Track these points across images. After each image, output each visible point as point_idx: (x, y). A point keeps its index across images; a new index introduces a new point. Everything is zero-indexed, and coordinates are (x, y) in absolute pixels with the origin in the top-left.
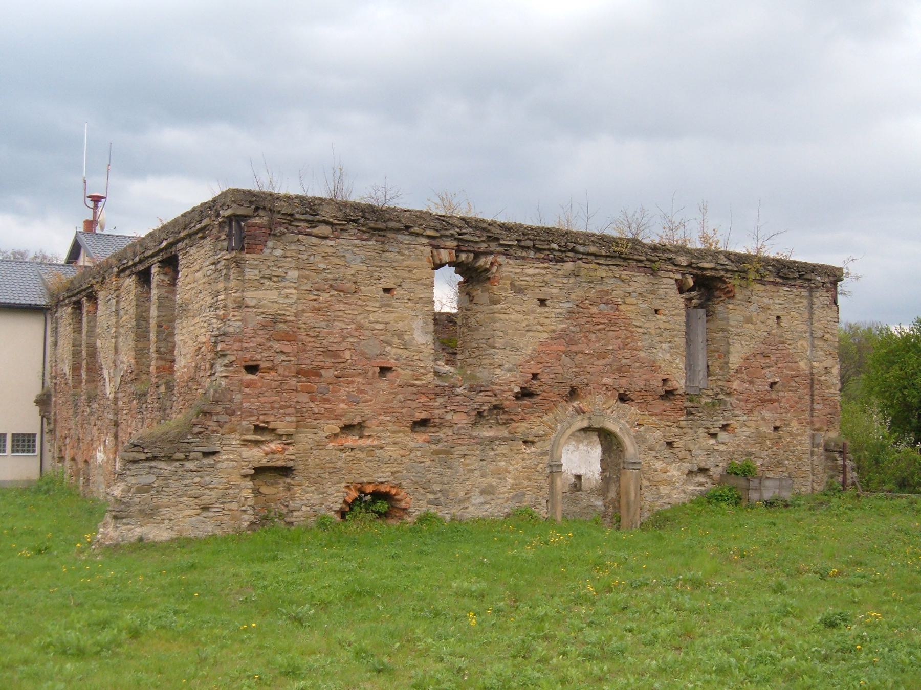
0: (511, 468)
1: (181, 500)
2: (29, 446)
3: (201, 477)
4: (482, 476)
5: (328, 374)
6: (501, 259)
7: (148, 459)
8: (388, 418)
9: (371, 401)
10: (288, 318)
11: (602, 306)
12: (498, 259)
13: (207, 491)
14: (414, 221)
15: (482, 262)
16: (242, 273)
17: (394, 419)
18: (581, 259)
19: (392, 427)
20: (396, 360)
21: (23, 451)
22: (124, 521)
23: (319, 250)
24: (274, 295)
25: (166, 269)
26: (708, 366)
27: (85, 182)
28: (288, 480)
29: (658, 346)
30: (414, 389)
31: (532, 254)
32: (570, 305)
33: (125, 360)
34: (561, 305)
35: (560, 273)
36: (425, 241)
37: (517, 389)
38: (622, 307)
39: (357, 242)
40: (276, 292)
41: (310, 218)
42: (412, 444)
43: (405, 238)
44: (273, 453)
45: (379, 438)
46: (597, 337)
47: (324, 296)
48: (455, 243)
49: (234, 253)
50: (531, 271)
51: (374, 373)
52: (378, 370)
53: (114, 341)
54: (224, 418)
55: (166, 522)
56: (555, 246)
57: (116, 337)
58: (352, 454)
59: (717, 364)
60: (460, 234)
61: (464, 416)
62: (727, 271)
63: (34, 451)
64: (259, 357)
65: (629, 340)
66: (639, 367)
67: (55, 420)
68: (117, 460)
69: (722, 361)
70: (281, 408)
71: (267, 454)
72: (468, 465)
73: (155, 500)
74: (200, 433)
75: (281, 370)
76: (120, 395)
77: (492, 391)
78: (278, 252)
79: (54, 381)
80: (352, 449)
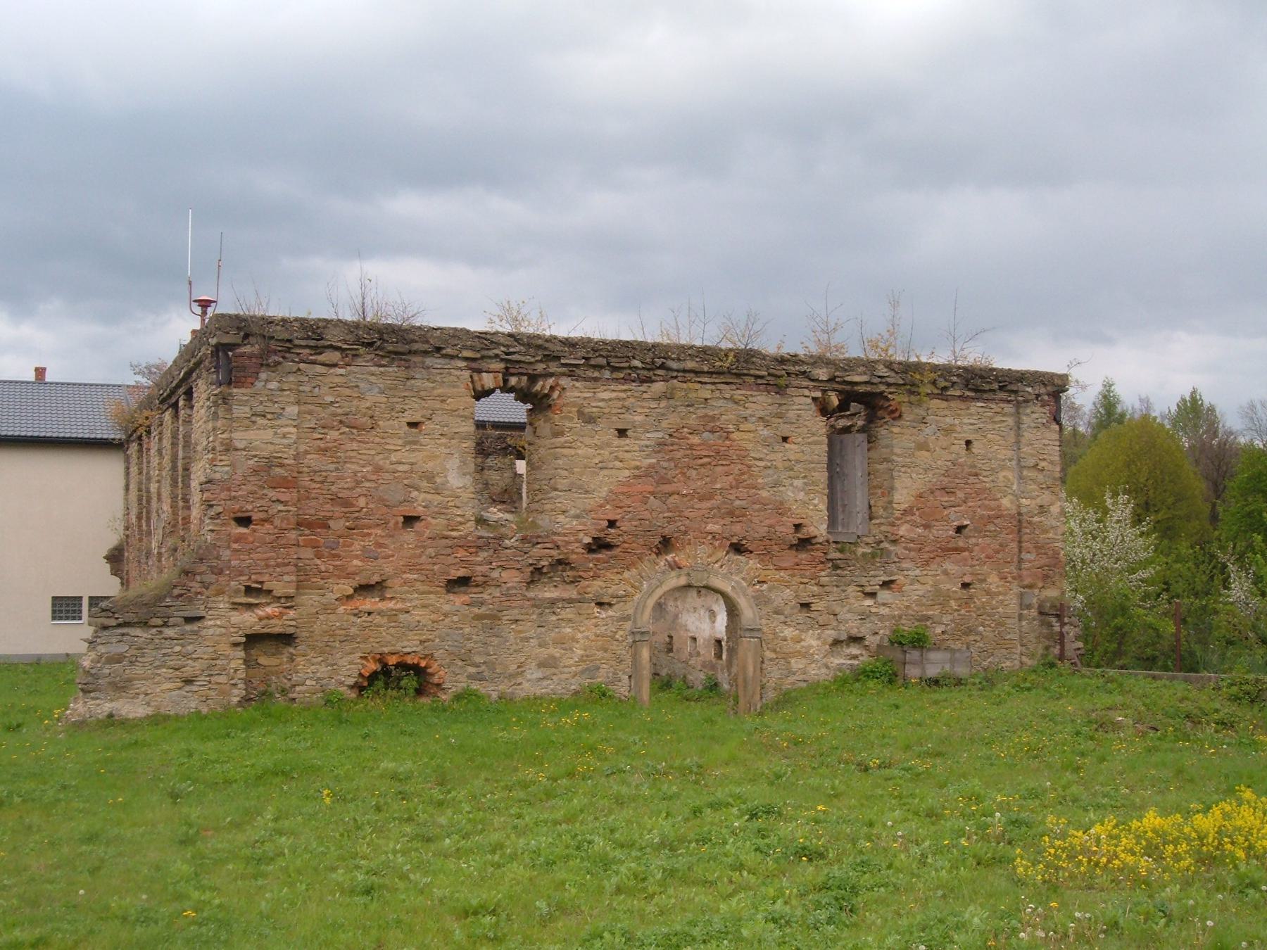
11: (706, 435)
13: (190, 662)
23: (327, 380)
24: (268, 435)
36: (462, 364)
40: (270, 431)
41: (312, 343)
45: (403, 600)
48: (502, 365)
51: (397, 523)
52: (401, 519)
54: (210, 578)
55: (142, 696)
64: (249, 507)
69: (886, 499)
70: (278, 565)
77: (553, 542)
78: (273, 385)
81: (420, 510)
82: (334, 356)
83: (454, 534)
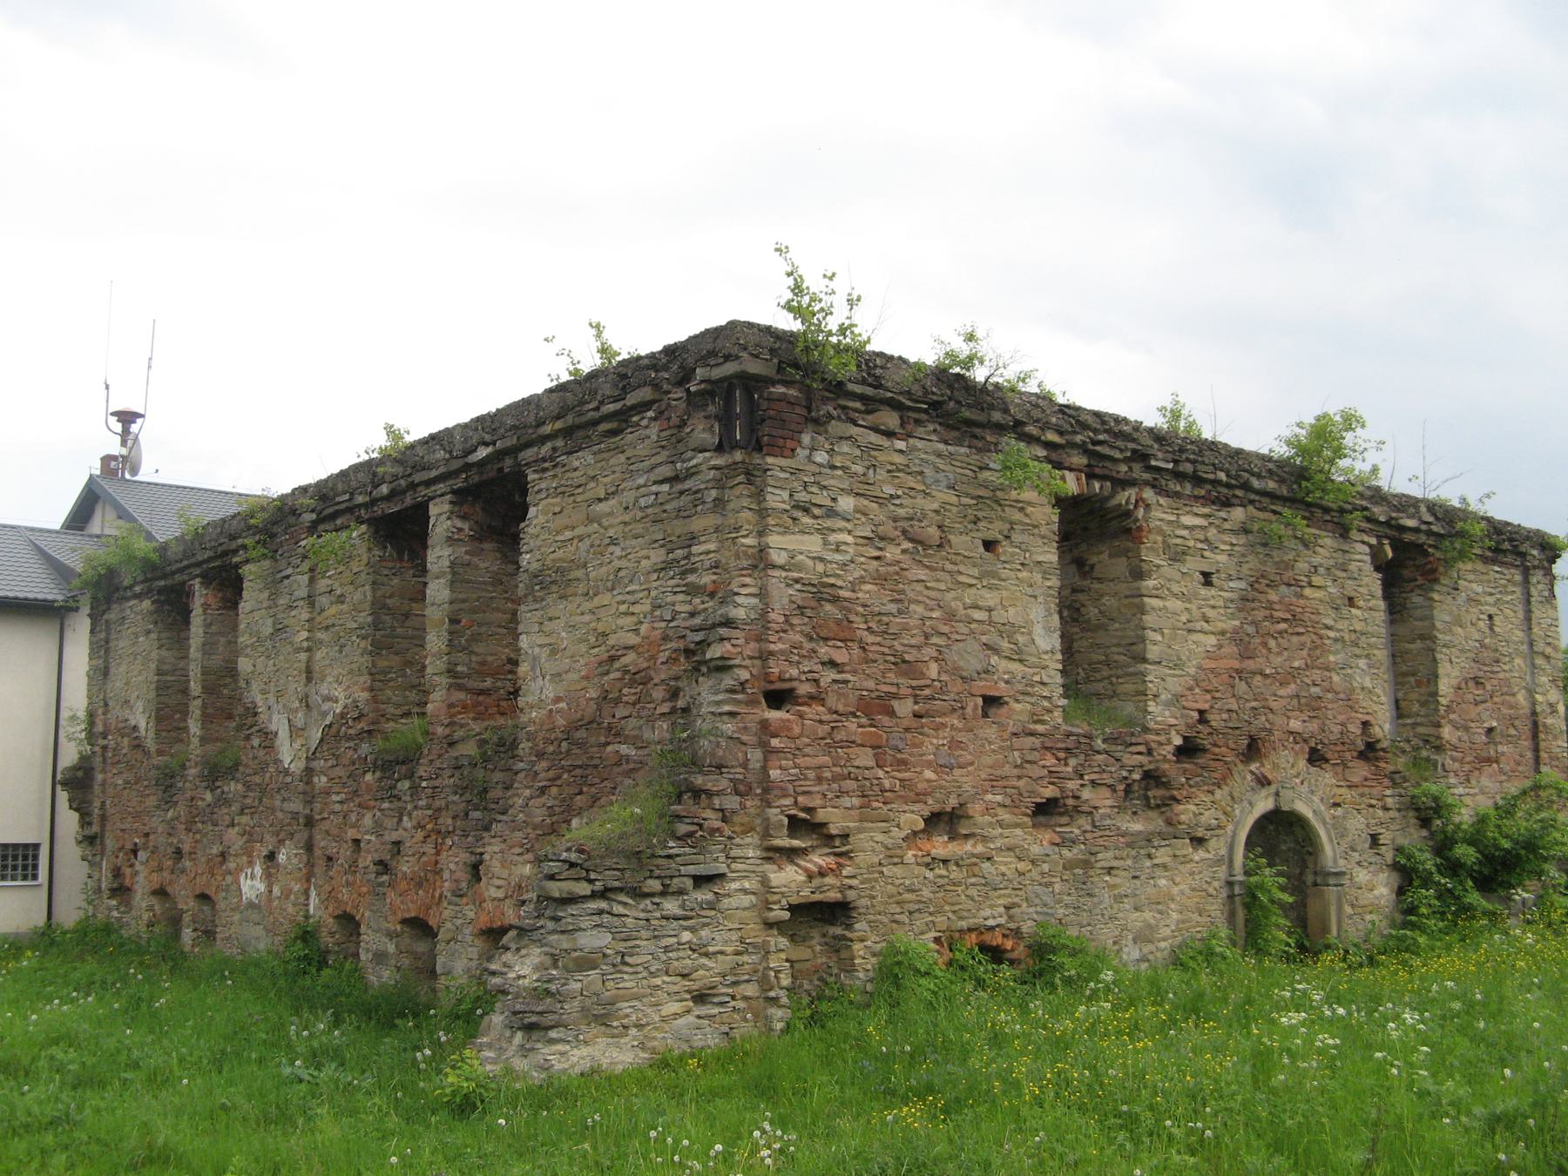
0: (1175, 890)
1: (658, 981)
2: (25, 868)
3: (692, 930)
4: (1136, 909)
5: (904, 708)
6: (1148, 494)
7: (594, 895)
8: (999, 798)
9: (972, 764)
10: (842, 593)
11: (1283, 588)
12: (1145, 495)
13: (704, 961)
14: (1028, 413)
15: (1126, 496)
16: (759, 495)
17: (1008, 801)
18: (1252, 502)
19: (1005, 816)
20: (1007, 682)
21: (14, 878)
22: (553, 1034)
23: (882, 457)
24: (813, 544)
25: (465, 508)
26: (1397, 701)
27: (107, 387)
28: (838, 931)
29: (1353, 661)
30: (1037, 742)
31: (1188, 489)
32: (1242, 585)
33: (339, 693)
34: (1232, 584)
35: (1227, 526)
36: (1042, 452)
37: (1178, 741)
38: (1308, 592)
39: (941, 446)
40: (817, 538)
41: (869, 391)
42: (1036, 849)
43: (1010, 442)
44: (822, 874)
45: (985, 839)
46: (1278, 645)
47: (892, 553)
48: (1085, 461)
49: (738, 456)
50: (1187, 520)
52: (980, 701)
53: (303, 656)
54: (731, 802)
55: (633, 1031)
56: (1222, 476)
57: (309, 649)
58: (944, 872)
59: (1413, 696)
60: (1095, 443)
61: (1106, 792)
62: (1430, 533)
63: (35, 877)
64: (794, 672)
65: (1318, 652)
66: (1332, 702)
67: (103, 818)
68: (313, 893)
69: (1423, 690)
70: (835, 779)
71: (810, 877)
72: (1114, 886)
73: (610, 984)
74: (691, 834)
75: (832, 701)
76: (317, 764)
77: (1146, 744)
78: (821, 457)
79: (102, 742)
80: (945, 862)
81: (1001, 689)
82: (891, 419)
83: (1040, 728)
